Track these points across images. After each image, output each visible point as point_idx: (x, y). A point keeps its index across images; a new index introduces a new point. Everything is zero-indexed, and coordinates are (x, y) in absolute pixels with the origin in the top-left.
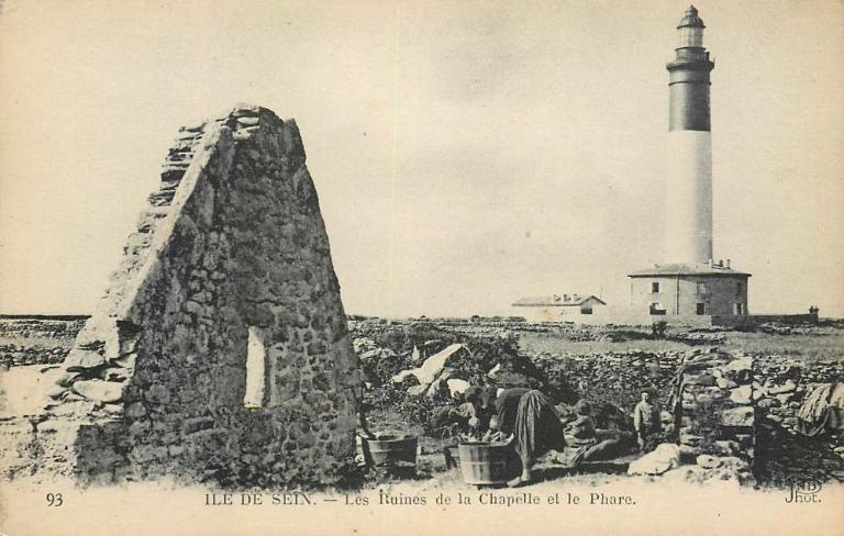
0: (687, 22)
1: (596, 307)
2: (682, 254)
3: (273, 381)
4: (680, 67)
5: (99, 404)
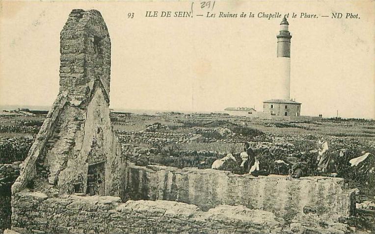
0: (283, 22)
1: (253, 111)
2: (280, 96)
3: (272, 104)
4: (282, 37)
5: (313, 130)
